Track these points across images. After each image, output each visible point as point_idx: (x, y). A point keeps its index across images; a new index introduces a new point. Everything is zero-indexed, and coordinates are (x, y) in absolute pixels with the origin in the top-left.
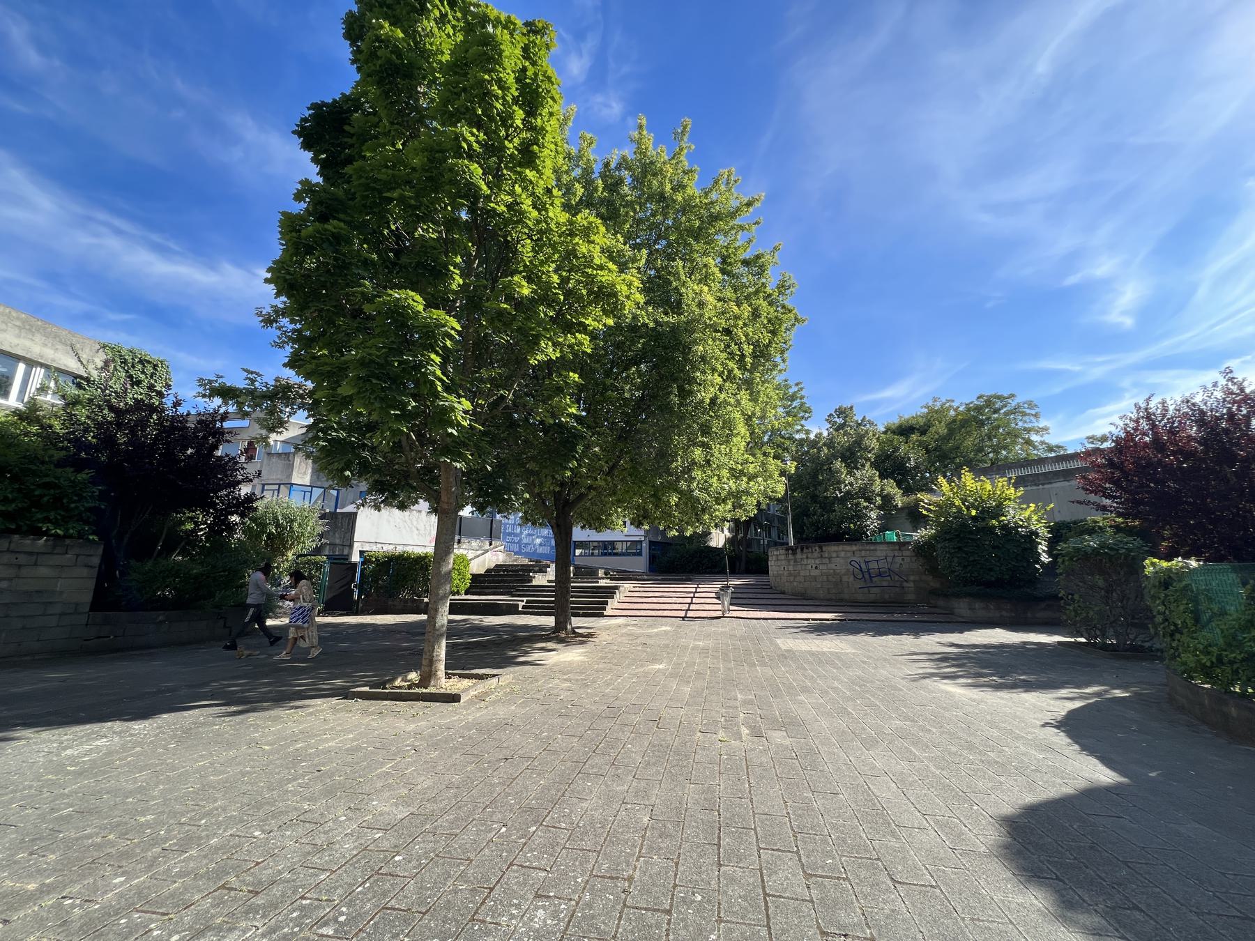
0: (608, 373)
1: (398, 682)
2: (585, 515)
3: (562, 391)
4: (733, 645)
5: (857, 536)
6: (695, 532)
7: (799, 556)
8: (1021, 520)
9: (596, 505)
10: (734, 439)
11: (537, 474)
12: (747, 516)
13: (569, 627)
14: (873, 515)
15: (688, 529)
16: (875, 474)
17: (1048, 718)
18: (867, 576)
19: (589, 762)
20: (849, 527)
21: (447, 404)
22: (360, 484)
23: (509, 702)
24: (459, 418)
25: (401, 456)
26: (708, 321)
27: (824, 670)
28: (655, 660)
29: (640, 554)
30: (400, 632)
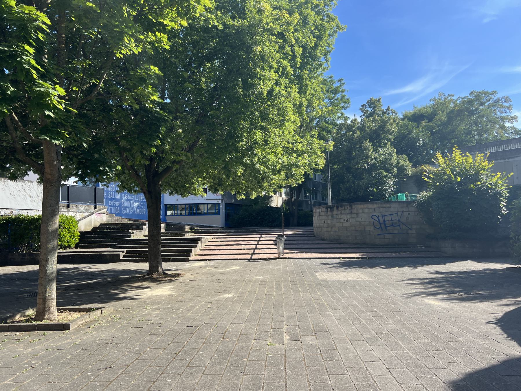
0: (187, 67)
1: (18, 318)
2: (172, 184)
3: (145, 81)
4: (284, 278)
5: (379, 197)
6: (258, 196)
7: (335, 212)
8: (491, 184)
9: (181, 175)
10: (286, 124)
11: (130, 150)
12: (297, 184)
13: (160, 270)
14: (391, 182)
15: (252, 194)
16: (393, 151)
17: (491, 318)
18: (383, 226)
19: (170, 366)
20: (373, 190)
21: (42, 90)
22: (109, 185)
23: (110, 328)
24: (55, 102)
25: (7, 135)
26: (266, 26)
27: (347, 293)
28: (226, 291)
29: (218, 213)
30: (19, 279)
